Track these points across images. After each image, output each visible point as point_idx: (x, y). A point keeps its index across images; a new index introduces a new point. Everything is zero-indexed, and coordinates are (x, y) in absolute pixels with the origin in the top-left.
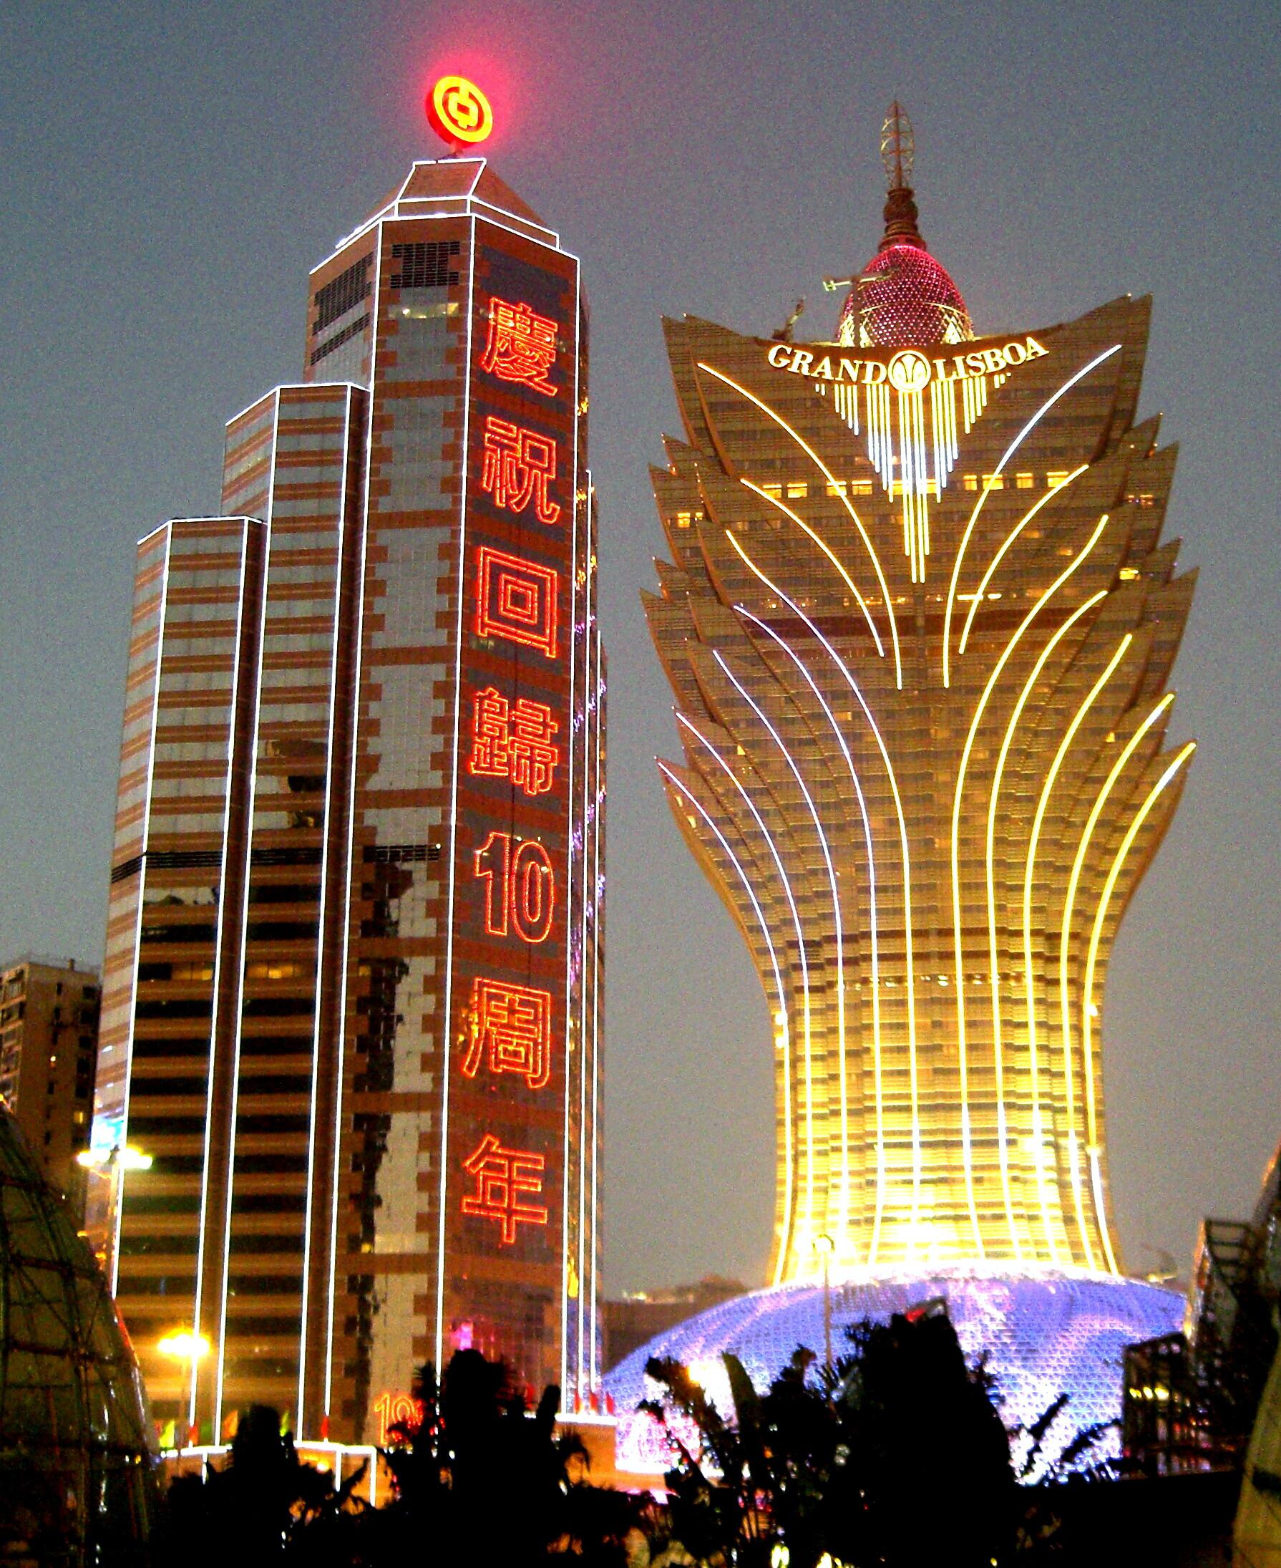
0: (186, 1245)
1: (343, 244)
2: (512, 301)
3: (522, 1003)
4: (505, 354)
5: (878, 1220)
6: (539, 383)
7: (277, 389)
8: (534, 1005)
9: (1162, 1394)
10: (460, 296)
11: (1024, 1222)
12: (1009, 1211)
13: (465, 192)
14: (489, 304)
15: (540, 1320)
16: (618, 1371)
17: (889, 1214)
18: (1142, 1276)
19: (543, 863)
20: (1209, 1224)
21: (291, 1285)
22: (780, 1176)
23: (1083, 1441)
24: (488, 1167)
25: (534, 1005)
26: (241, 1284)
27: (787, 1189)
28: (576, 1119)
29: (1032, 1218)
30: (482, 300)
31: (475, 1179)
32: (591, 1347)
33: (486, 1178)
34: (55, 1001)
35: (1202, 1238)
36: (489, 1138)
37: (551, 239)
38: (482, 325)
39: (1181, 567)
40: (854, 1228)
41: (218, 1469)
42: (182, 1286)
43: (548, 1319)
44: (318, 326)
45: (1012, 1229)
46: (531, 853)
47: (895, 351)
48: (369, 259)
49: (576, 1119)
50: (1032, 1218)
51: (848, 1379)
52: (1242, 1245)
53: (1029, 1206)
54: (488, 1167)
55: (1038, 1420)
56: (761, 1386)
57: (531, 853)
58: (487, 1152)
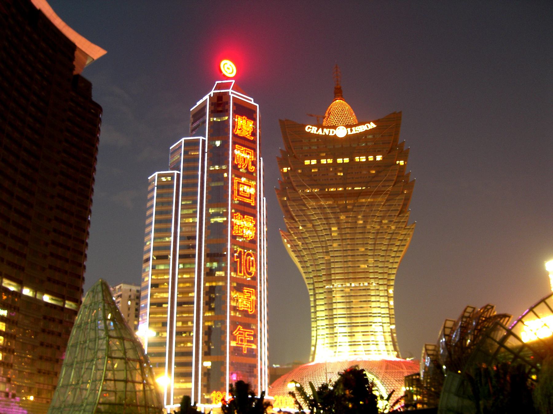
0: (163, 355)
1: (198, 103)
2: (242, 115)
4: (240, 129)
5: (338, 346)
6: (248, 137)
7: (183, 140)
8: (250, 293)
9: (415, 389)
10: (229, 115)
11: (375, 345)
12: (371, 343)
13: (229, 89)
14: (247, 351)
15: (253, 372)
16: (273, 384)
17: (340, 344)
18: (405, 359)
19: (252, 257)
20: (426, 345)
21: (190, 364)
22: (312, 335)
23: (397, 402)
24: (239, 334)
25: (250, 293)
26: (178, 364)
27: (315, 338)
28: (261, 320)
29: (377, 344)
30: (234, 117)
31: (236, 337)
32: (266, 379)
34: (129, 293)
35: (424, 349)
36: (239, 326)
37: (251, 101)
38: (234, 122)
39: (410, 180)
40: (332, 348)
41: (177, 411)
42: (162, 365)
43: (255, 372)
44: (193, 123)
45: (372, 347)
46: (249, 255)
47: (337, 126)
48: (206, 106)
49: (261, 320)
50: (377, 344)
51: (492, 374)
52: (434, 350)
53: (376, 341)
54: (239, 334)
55: (218, 392)
56: (317, 389)
57: (249, 255)
58: (239, 330)
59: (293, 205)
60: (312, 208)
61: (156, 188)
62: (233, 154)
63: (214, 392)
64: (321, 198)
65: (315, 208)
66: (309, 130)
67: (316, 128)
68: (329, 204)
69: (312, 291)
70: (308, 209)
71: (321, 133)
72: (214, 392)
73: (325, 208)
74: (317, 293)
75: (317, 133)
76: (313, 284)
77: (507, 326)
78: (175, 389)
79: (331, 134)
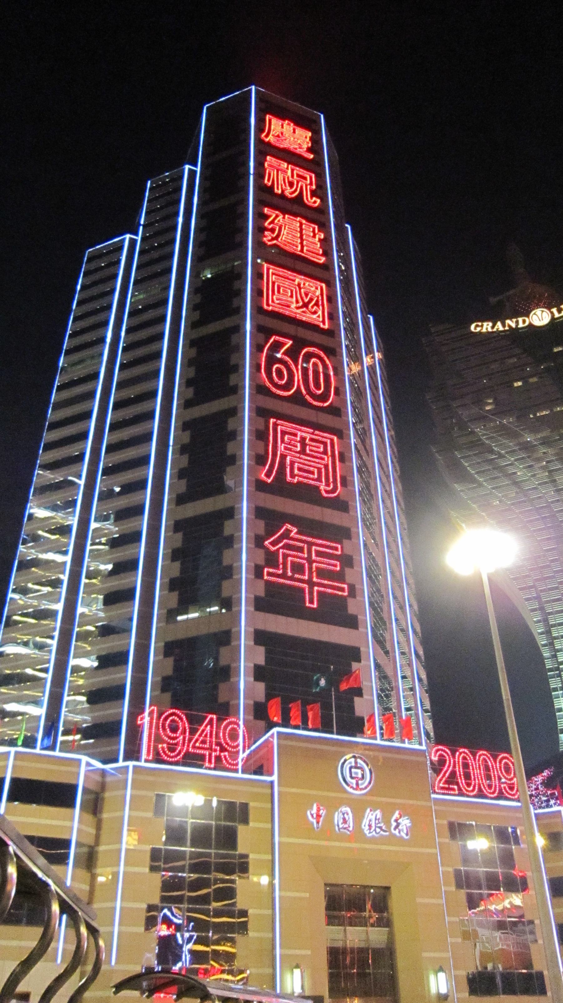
3: (312, 440)
33: (285, 556)
59: (469, 456)
60: (507, 453)
61: (141, 228)
62: (272, 875)
63: (409, 825)
64: (522, 430)
65: (514, 451)
66: (478, 329)
67: (491, 324)
68: (543, 438)
69: (538, 612)
70: (501, 456)
71: (501, 329)
72: (409, 825)
73: (536, 445)
74: (550, 614)
75: (495, 330)
76: (538, 598)
77: (289, 991)
78: (189, 864)
79: (521, 325)
